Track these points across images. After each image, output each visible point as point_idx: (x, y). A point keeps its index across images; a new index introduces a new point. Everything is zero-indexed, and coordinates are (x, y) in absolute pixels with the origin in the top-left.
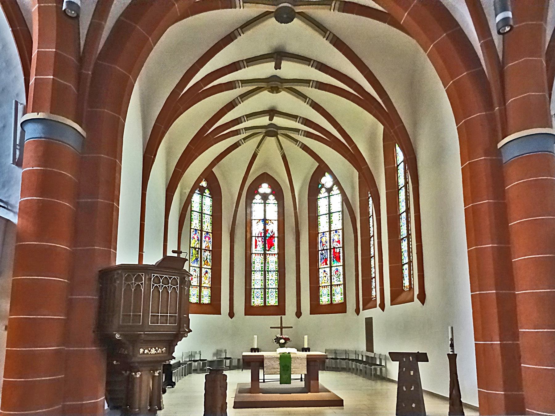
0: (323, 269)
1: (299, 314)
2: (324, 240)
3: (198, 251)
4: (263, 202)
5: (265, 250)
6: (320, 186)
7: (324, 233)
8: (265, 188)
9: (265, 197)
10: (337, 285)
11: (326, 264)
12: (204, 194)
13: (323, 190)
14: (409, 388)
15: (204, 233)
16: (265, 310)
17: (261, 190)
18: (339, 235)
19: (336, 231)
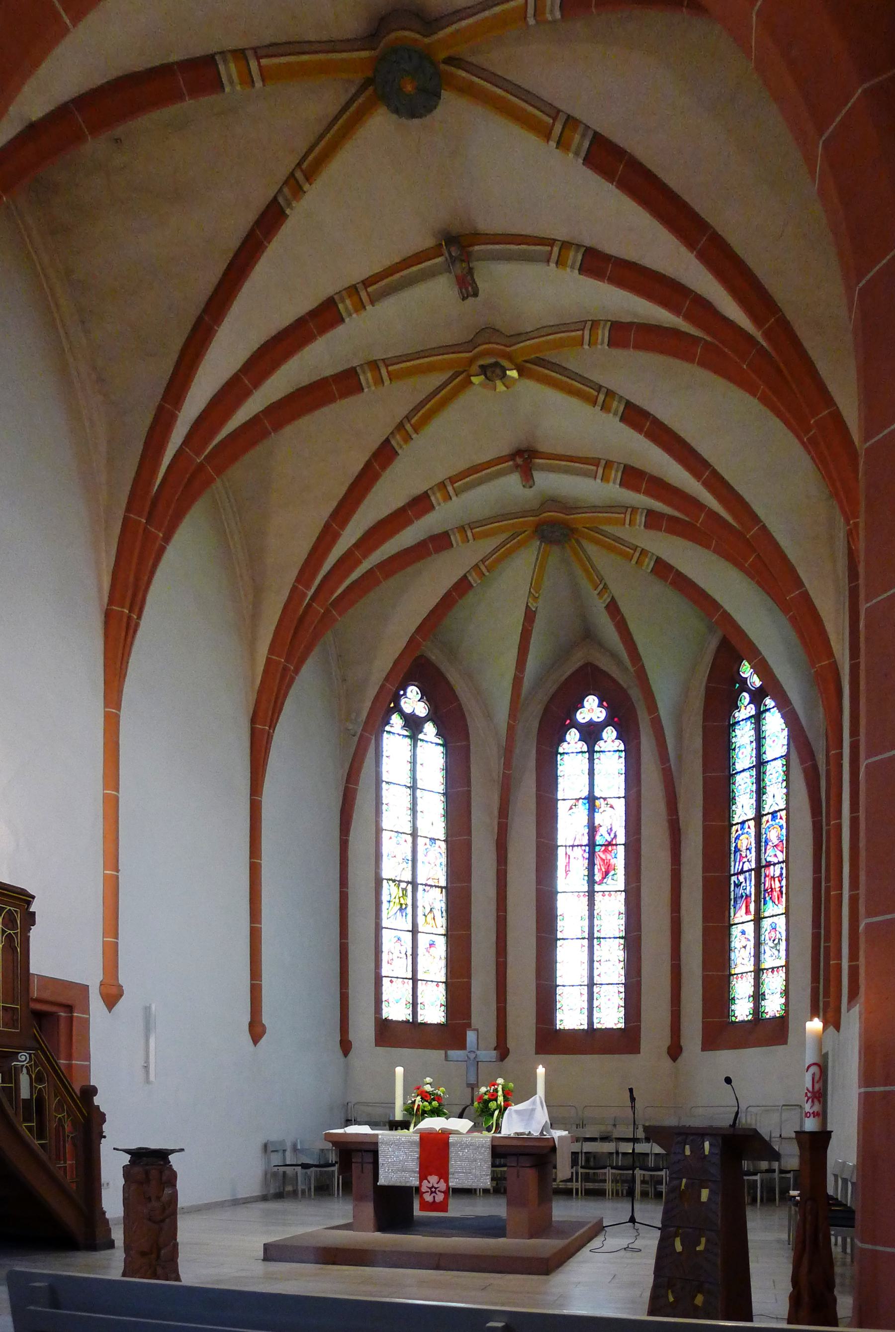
1: (675, 1051)
3: (405, 890)
4: (585, 748)
5: (591, 881)
7: (743, 823)
8: (592, 710)
9: (413, 725)
14: (690, 1243)
15: (420, 841)
16: (592, 1040)
17: (582, 716)
18: (781, 827)
19: (774, 814)
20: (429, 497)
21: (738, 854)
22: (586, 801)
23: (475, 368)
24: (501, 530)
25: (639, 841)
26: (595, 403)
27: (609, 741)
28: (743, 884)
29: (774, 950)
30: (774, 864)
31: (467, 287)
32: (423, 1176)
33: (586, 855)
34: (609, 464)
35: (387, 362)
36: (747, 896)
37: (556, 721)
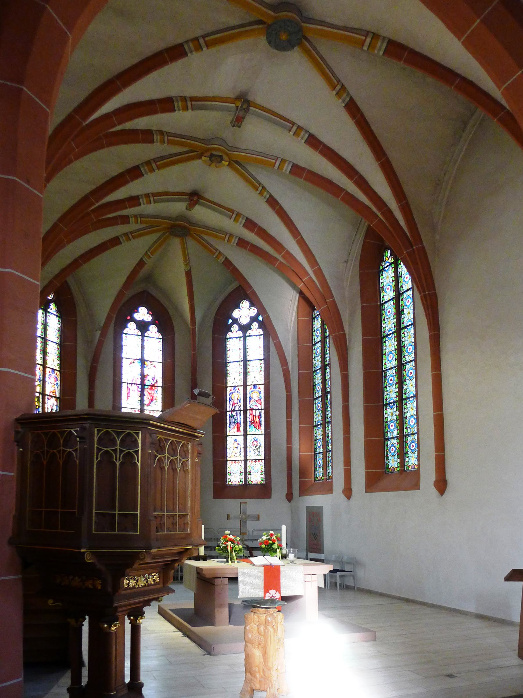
0: (234, 438)
2: (235, 397)
6: (230, 321)
7: (235, 387)
8: (143, 314)
9: (143, 327)
10: (255, 460)
11: (238, 430)
12: (49, 310)
13: (235, 327)
15: (48, 370)
17: (137, 316)
18: (260, 393)
19: (255, 386)
20: (139, 199)
21: (232, 402)
22: (140, 361)
23: (208, 154)
24: (202, 238)
25: (173, 387)
26: (257, 190)
27: (154, 332)
28: (235, 416)
29: (256, 451)
30: (255, 410)
31: (238, 122)
32: (266, 591)
33: (140, 390)
34: (238, 215)
35: (169, 134)
36: (238, 423)
37: (121, 316)
